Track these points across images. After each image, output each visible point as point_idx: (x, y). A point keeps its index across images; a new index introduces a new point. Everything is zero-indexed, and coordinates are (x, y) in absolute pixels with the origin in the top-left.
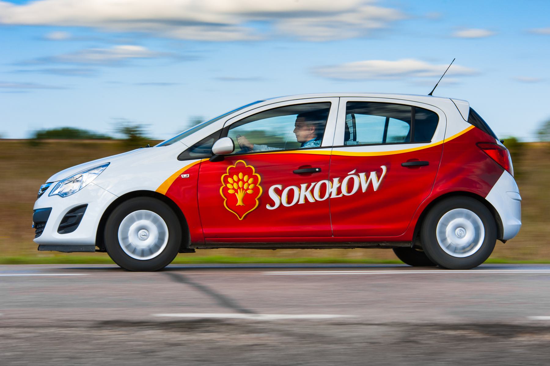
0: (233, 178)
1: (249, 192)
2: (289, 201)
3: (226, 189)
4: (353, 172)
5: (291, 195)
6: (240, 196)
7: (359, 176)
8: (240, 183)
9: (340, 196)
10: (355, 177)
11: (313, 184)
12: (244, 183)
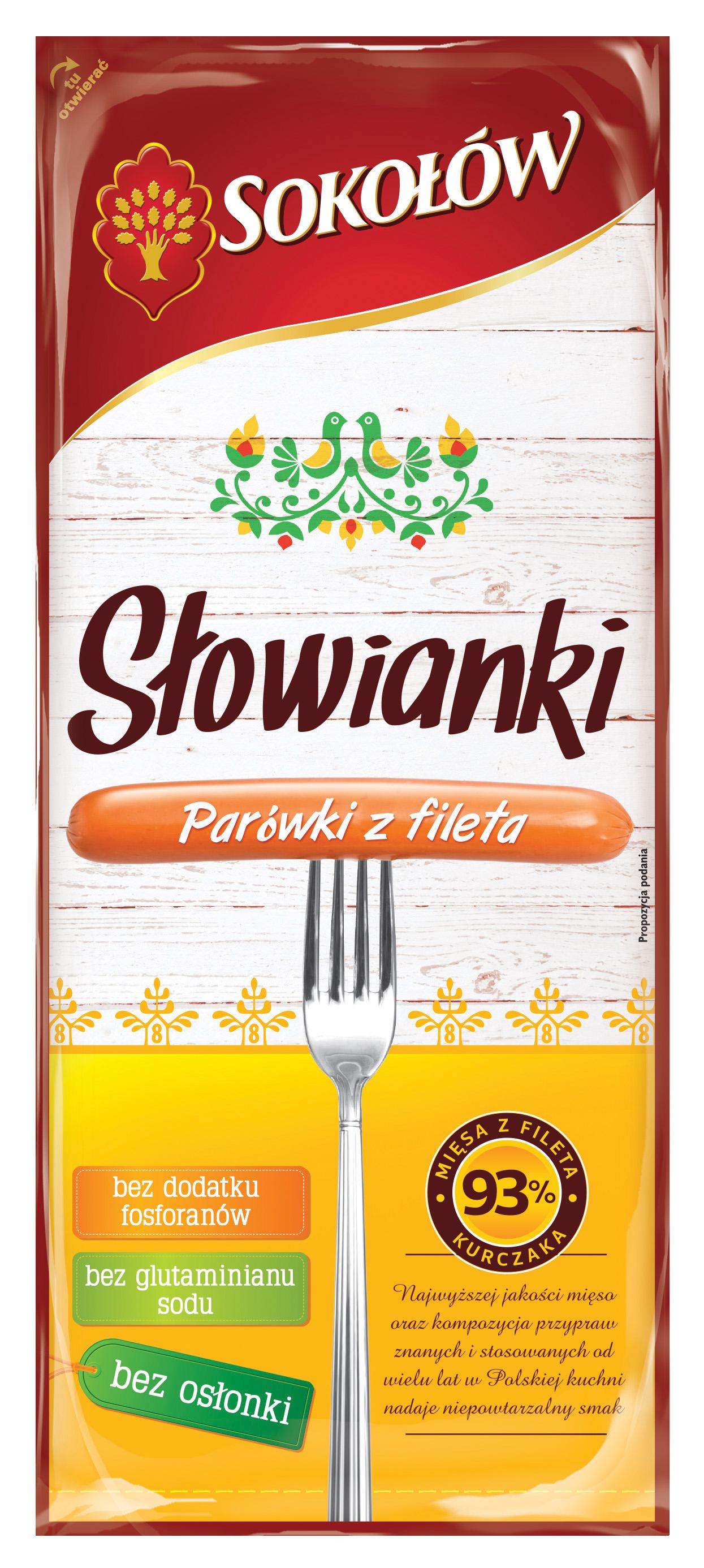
0: (178, 199)
1: (182, 238)
2: (390, 179)
3: (111, 230)
4: (482, 133)
5: (291, 203)
6: (152, 253)
8: (153, 215)
9: (446, 206)
10: (487, 150)
11: (357, 172)
12: (164, 211)
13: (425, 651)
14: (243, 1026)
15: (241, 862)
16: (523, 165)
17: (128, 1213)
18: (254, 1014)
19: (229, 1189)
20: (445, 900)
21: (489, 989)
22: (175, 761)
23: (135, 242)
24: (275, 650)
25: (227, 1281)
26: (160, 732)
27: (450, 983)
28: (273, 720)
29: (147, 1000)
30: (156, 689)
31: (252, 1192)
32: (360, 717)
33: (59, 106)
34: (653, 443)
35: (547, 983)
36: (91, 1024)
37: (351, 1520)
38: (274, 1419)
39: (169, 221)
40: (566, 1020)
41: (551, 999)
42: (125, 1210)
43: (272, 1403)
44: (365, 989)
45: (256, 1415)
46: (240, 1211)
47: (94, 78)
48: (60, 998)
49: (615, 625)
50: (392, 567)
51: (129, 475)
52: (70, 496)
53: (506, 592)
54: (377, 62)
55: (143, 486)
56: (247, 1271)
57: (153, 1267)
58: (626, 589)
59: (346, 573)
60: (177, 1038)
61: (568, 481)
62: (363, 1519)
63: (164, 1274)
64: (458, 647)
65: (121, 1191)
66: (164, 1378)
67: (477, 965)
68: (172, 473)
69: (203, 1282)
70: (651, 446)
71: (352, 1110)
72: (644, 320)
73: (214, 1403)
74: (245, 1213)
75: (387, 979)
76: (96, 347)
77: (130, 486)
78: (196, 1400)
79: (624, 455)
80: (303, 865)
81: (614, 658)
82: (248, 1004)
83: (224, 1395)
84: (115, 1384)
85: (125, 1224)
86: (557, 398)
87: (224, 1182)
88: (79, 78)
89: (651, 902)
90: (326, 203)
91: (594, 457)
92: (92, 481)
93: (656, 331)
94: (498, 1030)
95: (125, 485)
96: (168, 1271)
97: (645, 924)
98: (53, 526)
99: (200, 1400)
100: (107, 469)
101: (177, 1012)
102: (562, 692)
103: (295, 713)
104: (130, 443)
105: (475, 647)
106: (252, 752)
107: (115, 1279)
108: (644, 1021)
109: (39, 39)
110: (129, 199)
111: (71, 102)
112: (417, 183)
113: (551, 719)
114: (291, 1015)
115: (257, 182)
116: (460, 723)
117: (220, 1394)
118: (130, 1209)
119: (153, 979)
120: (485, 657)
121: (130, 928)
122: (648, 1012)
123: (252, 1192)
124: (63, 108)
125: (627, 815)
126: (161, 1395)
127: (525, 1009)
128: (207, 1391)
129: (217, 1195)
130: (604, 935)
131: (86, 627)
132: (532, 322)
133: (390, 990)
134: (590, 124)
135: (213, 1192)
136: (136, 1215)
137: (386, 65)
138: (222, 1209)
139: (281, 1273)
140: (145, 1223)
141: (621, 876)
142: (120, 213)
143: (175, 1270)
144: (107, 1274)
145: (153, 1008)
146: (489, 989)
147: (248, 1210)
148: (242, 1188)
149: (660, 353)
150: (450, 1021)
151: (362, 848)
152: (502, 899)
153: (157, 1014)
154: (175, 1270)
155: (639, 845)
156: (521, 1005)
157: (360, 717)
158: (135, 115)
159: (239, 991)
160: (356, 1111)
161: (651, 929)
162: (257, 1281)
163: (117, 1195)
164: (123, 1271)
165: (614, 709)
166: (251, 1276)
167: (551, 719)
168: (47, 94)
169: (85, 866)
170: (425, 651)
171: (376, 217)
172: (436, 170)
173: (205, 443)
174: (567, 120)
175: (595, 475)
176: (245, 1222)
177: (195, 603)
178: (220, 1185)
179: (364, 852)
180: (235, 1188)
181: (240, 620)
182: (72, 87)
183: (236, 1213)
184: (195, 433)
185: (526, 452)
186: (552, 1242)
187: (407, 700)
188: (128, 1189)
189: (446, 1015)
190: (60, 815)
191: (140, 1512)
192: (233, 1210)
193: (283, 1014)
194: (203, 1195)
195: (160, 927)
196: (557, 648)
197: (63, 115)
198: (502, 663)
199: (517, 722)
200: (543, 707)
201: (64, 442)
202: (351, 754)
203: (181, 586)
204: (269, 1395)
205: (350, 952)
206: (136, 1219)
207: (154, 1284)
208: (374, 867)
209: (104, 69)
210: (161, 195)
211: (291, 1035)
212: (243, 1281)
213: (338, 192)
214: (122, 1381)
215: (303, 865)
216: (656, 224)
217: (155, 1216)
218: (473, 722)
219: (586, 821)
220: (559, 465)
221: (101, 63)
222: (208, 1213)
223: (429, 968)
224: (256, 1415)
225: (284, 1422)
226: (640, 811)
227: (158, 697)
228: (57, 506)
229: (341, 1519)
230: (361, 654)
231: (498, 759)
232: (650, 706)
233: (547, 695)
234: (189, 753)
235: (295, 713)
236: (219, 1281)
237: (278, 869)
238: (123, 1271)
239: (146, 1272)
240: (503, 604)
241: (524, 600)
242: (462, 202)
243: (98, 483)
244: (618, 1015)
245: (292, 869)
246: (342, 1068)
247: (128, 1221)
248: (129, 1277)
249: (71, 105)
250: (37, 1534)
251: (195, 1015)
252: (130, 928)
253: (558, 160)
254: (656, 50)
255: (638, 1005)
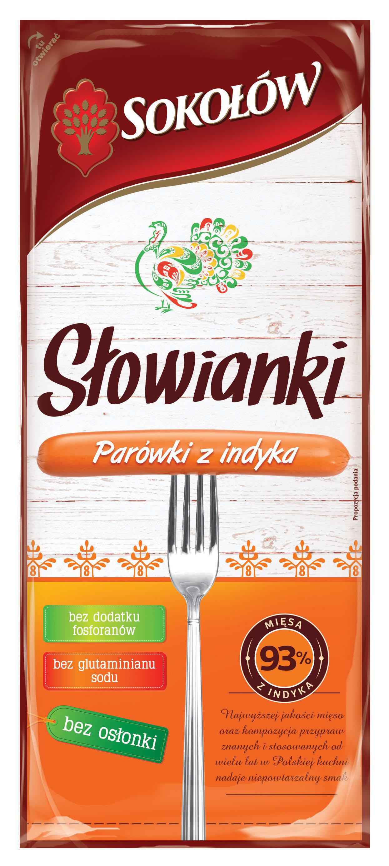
0: (99, 110)
3: (62, 127)
4: (267, 74)
6: (84, 140)
7: (276, 83)
8: (85, 119)
9: (247, 114)
10: (269, 83)
11: (197, 95)
12: (91, 117)
13: (235, 359)
14: (134, 566)
15: (133, 476)
16: (289, 92)
17: (76, 629)
18: (140, 560)
19: (125, 617)
20: (246, 497)
21: (270, 546)
22: (97, 419)
23: (75, 134)
24: (152, 359)
25: (122, 666)
26: (89, 404)
27: (249, 543)
28: (151, 397)
29: (81, 552)
30: (86, 381)
31: (136, 619)
32: (199, 396)
33: (33, 58)
34: (361, 244)
35: (302, 543)
36: (50, 566)
37: (194, 840)
38: (148, 747)
39: (94, 122)
40: (313, 563)
41: (303, 551)
42: (74, 628)
43: (147, 739)
44: (201, 546)
45: (138, 745)
46: (131, 628)
47: (52, 43)
48: (33, 551)
49: (340, 345)
50: (216, 313)
51: (71, 262)
52: (39, 273)
53: (279, 327)
54: (208, 34)
55: (79, 268)
56: (132, 662)
57: (87, 660)
58: (346, 325)
59: (191, 316)
60: (98, 574)
61: (314, 265)
62: (201, 839)
63: (92, 663)
64: (253, 357)
65: (72, 619)
66: (91, 726)
67: (264, 533)
68: (95, 261)
69: (111, 667)
70: (360, 246)
71: (194, 613)
72: (356, 176)
73: (116, 739)
74: (133, 629)
75: (214, 540)
76: (53, 193)
77: (72, 268)
78: (107, 737)
79: (345, 251)
80: (168, 478)
81: (339, 363)
82: (137, 555)
83: (122, 734)
84: (65, 729)
85: (74, 634)
86: (307, 219)
87: (123, 614)
88: (43, 43)
89: (360, 498)
90: (180, 113)
91: (328, 252)
92: (50, 266)
93: (362, 183)
94: (275, 570)
95: (69, 268)
96: (94, 662)
97: (356, 510)
98: (29, 290)
99: (109, 737)
100: (59, 259)
101: (98, 559)
102: (310, 382)
103: (163, 394)
104: (72, 245)
105: (263, 357)
106: (139, 414)
107: (67, 666)
108: (356, 564)
109: (22, 22)
110: (71, 110)
111: (39, 56)
112: (231, 101)
113: (305, 397)
114: (161, 560)
115: (142, 101)
116: (254, 400)
117: (119, 734)
118: (77, 627)
119: (85, 541)
120: (268, 363)
121: (72, 512)
122: (359, 559)
123: (136, 619)
124: (35, 60)
125: (347, 450)
126: (89, 735)
127: (290, 558)
128: (113, 732)
129: (119, 620)
130: (334, 517)
131: (47, 347)
132: (294, 178)
133: (216, 546)
134: (327, 66)
135: (117, 619)
136: (80, 630)
137: (213, 36)
138: (122, 627)
139: (149, 663)
140: (84, 634)
141: (344, 483)
142: (67, 117)
143: (97, 661)
144: (64, 663)
145: (84, 557)
146: (270, 546)
147: (134, 628)
148: (132, 617)
149: (365, 195)
150: (249, 564)
151: (199, 466)
152: (278, 497)
153: (87, 560)
154: (97, 661)
155: (353, 467)
156: (288, 555)
157: (199, 396)
158: (74, 64)
159: (132, 547)
160: (196, 613)
161: (360, 513)
162: (137, 666)
163: (70, 620)
164: (72, 662)
165: (340, 391)
166: (134, 664)
167: (304, 397)
168: (26, 52)
169: (46, 478)
170: (235, 359)
171: (208, 121)
172: (241, 94)
173: (113, 245)
174: (314, 67)
175: (328, 262)
176: (133, 634)
177: (108, 333)
178: (121, 616)
179: (201, 470)
180: (128, 617)
181: (133, 342)
182: (40, 48)
183: (129, 629)
184: (107, 239)
185: (291, 250)
186: (305, 688)
187: (225, 386)
188: (76, 618)
189: (246, 561)
190: (33, 450)
191: (77, 835)
192: (127, 628)
193: (157, 560)
194: (112, 620)
195: (88, 512)
196: (308, 358)
197: (35, 63)
198: (277, 366)
199: (286, 399)
200: (300, 391)
201: (36, 243)
202: (192, 415)
203: (100, 323)
204: (145, 735)
205: (194, 526)
206: (80, 633)
207: (87, 668)
208: (207, 479)
209: (58, 38)
210: (89, 107)
211: (160, 572)
212: (130, 666)
213: (187, 107)
214: (69, 727)
215: (168, 478)
216: (362, 124)
217: (89, 631)
218: (261, 399)
219: (323, 453)
220: (309, 256)
221: (56, 35)
222: (115, 629)
223: (237, 534)
224: (138, 745)
225: (153, 748)
226: (354, 448)
227: (87, 385)
228: (30, 281)
229: (189, 839)
230: (200, 361)
231: (274, 418)
232: (359, 390)
233: (302, 384)
234: (104, 412)
235: (163, 394)
236: (118, 667)
237: (153, 480)
238: (72, 662)
239: (83, 662)
240: (278, 333)
241: (290, 331)
242: (256, 112)
243: (54, 267)
244: (342, 560)
245: (161, 480)
246: (188, 589)
247: (76, 633)
248: (75, 665)
249: (39, 58)
250: (21, 847)
251: (107, 561)
252: (72, 512)
253: (309, 89)
254: (363, 27)
255: (353, 555)
